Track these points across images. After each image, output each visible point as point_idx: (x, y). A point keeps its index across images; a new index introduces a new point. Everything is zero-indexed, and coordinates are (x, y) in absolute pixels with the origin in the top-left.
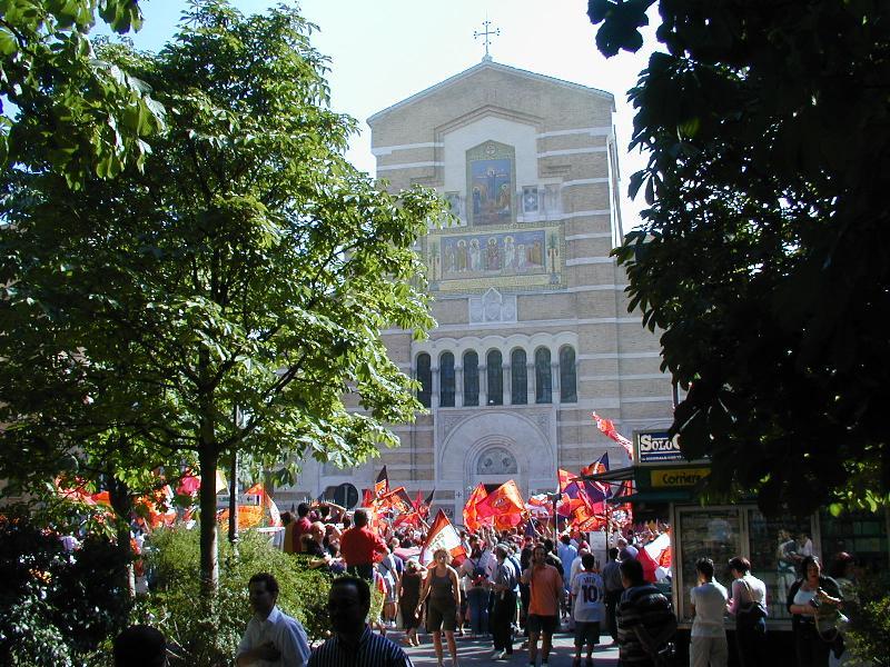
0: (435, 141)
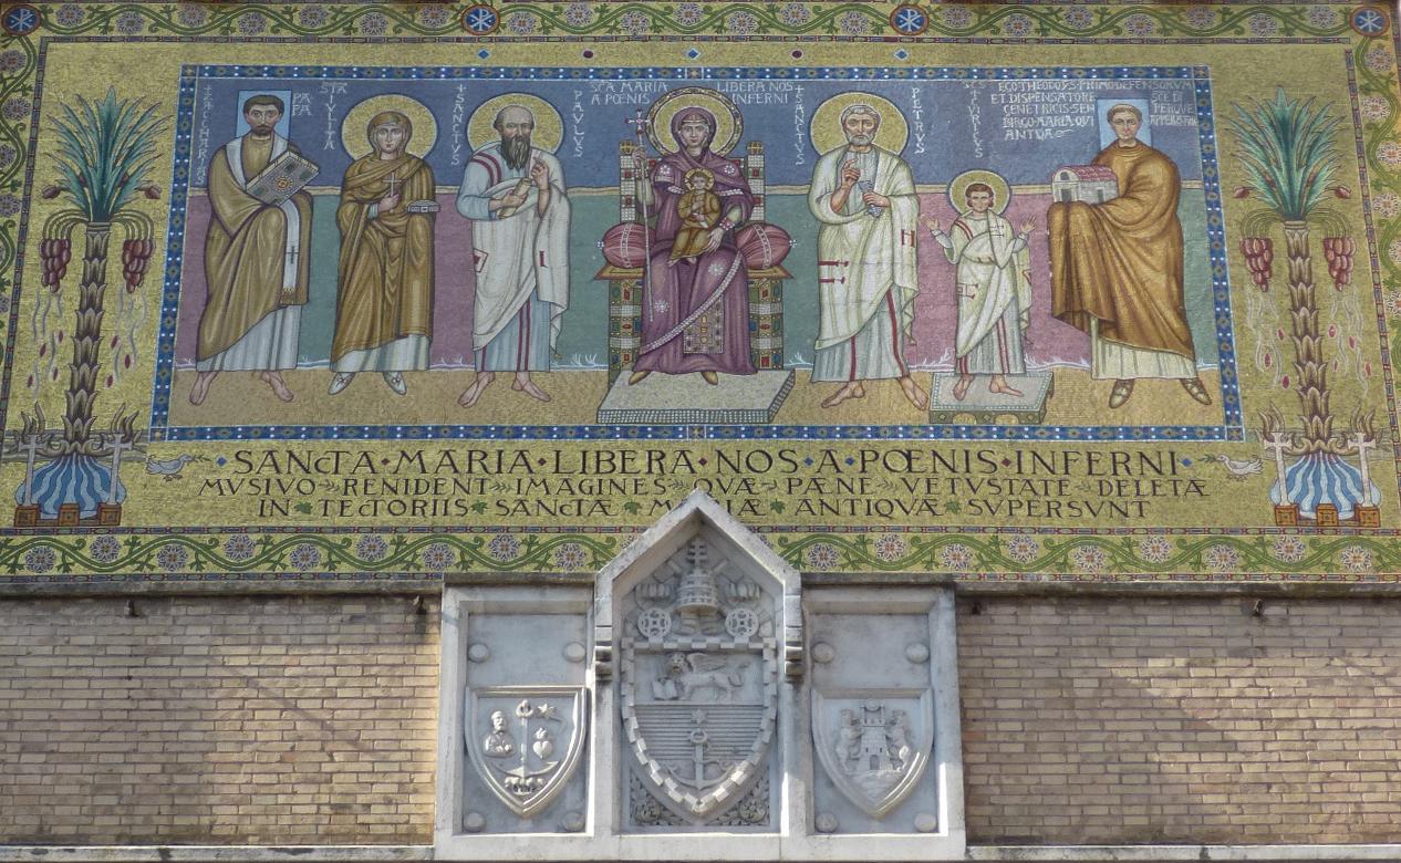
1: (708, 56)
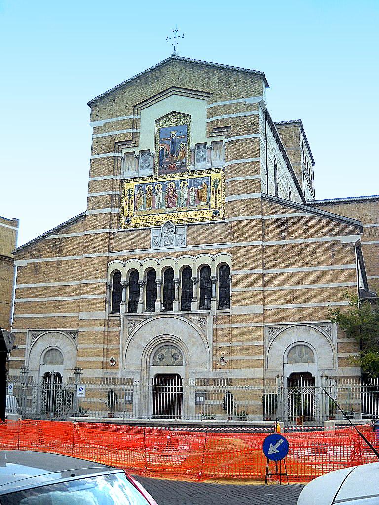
1: (173, 179)
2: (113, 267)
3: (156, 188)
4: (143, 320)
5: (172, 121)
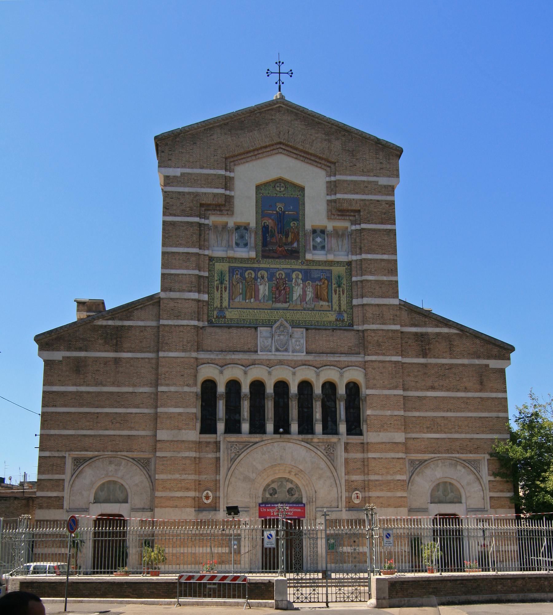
0: (226, 170)
2: (207, 372)
3: (259, 275)
4: (251, 444)
5: (278, 189)
